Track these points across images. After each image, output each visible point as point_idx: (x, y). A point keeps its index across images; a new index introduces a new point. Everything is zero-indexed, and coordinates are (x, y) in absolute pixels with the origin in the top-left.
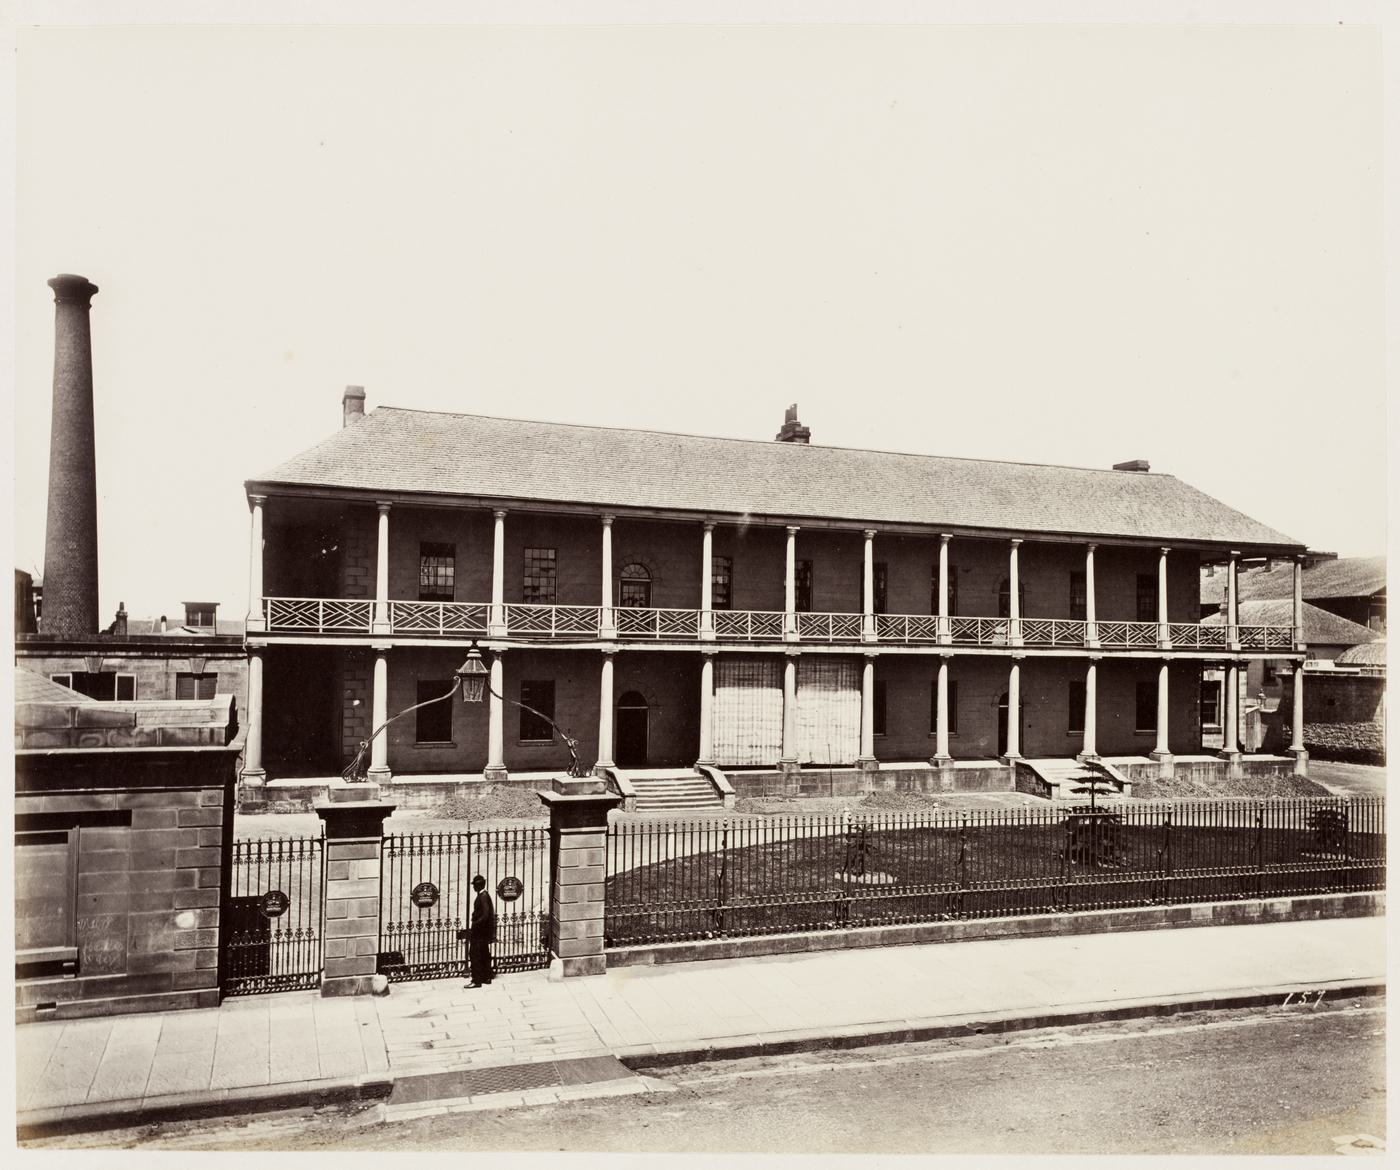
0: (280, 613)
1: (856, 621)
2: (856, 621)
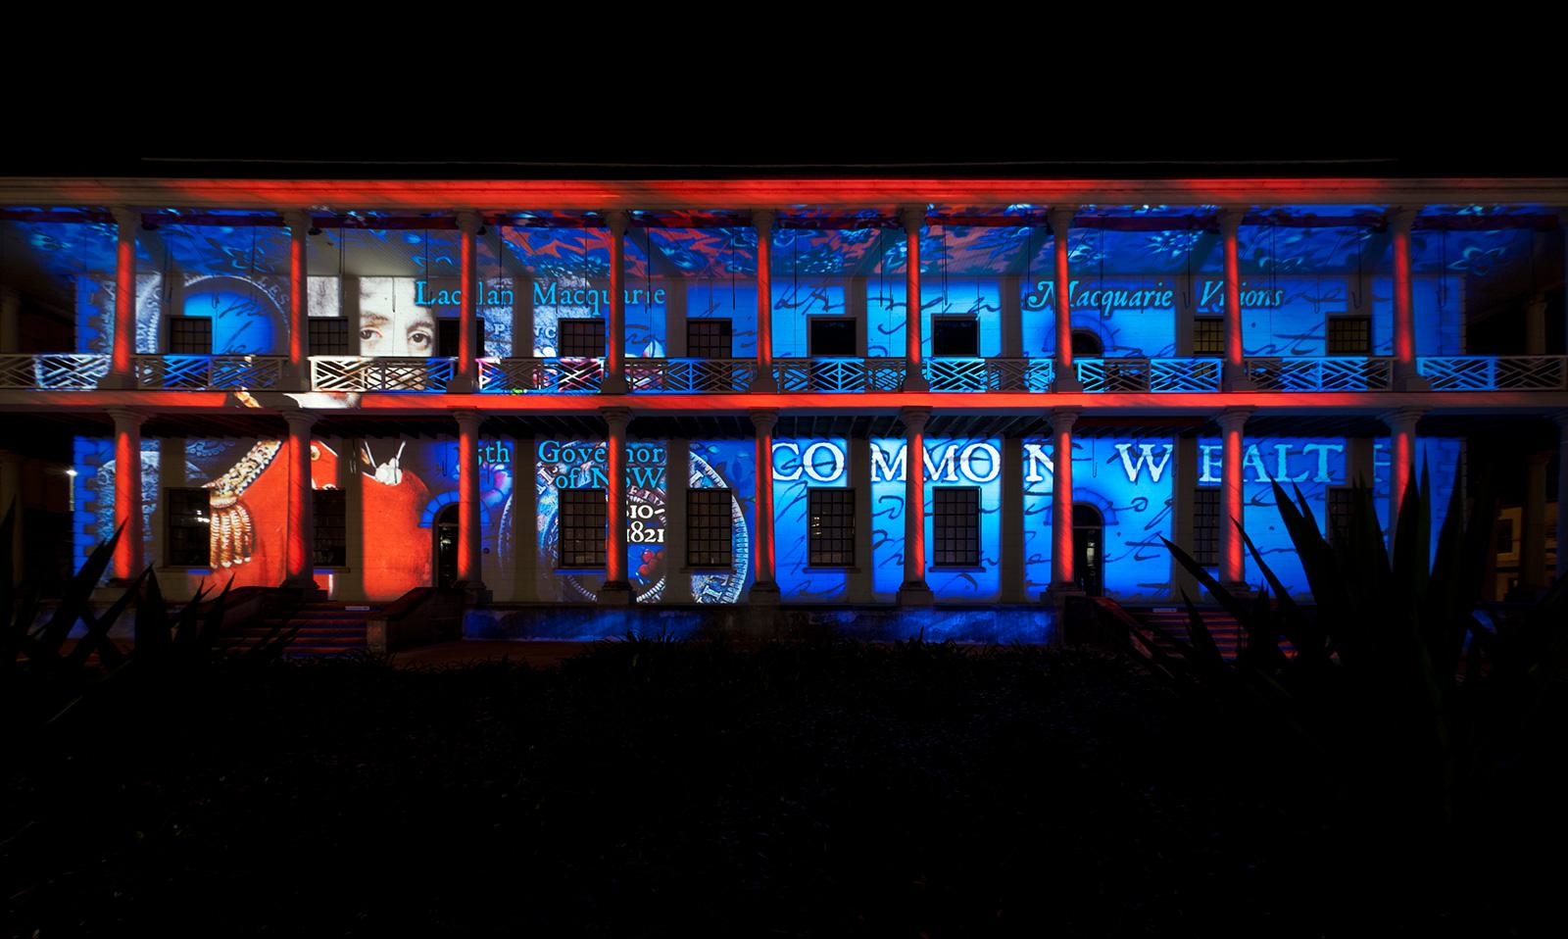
0: (1545, 377)
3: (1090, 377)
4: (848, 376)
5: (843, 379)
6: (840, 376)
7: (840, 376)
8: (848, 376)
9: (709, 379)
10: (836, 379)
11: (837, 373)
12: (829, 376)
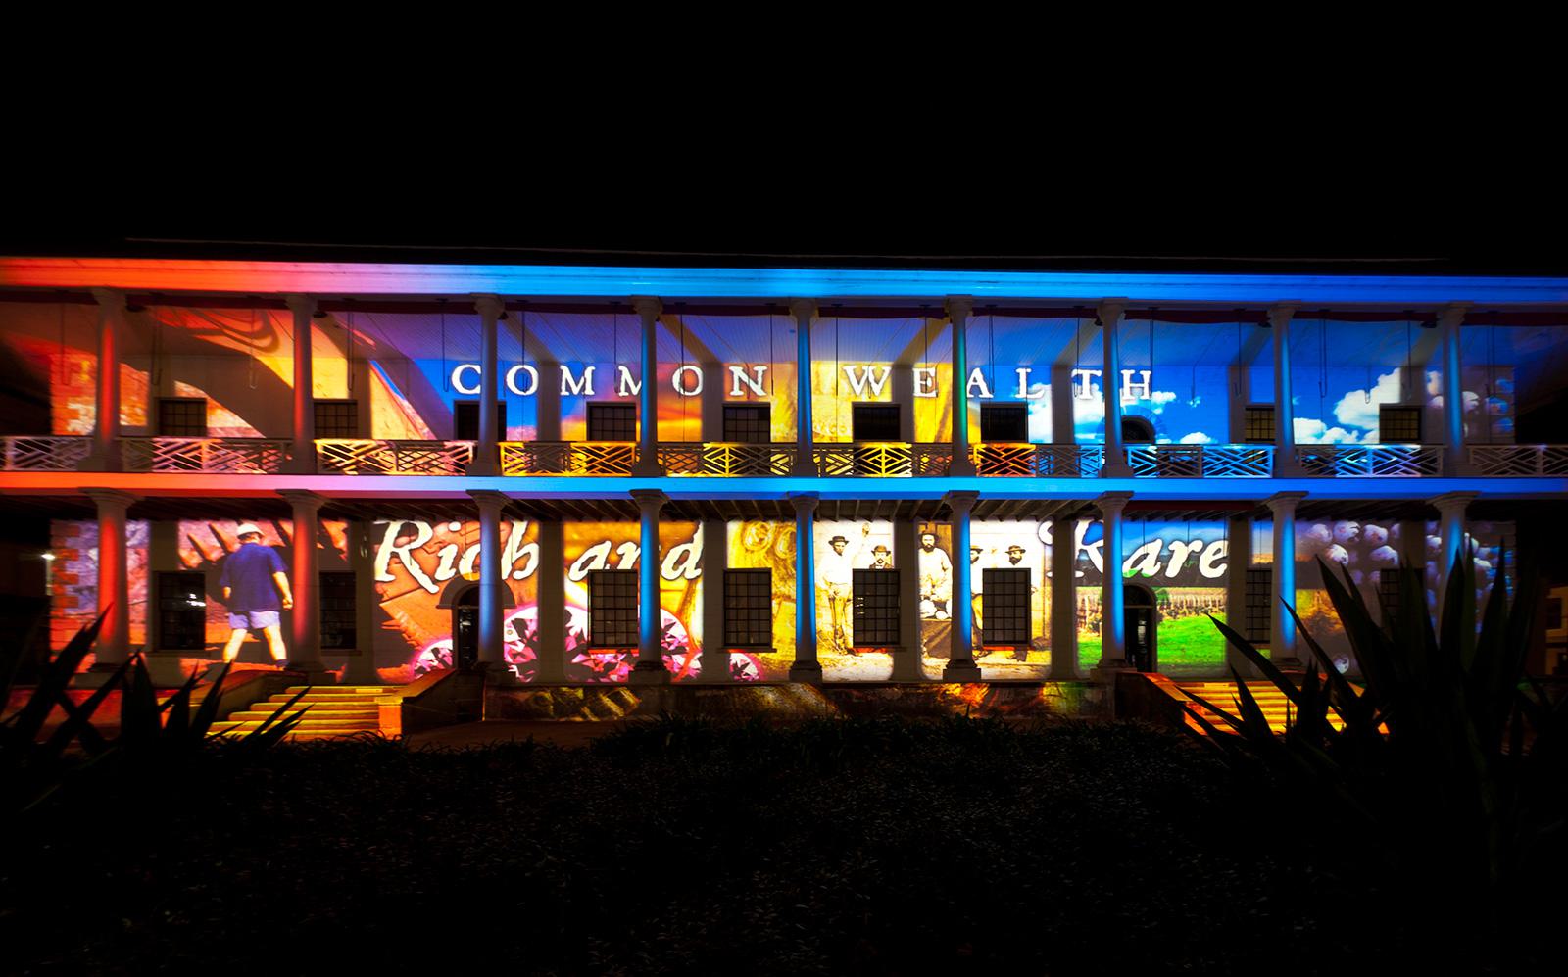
1: (23, 461)
2: (23, 461)
3: (1140, 463)
4: (892, 461)
5: (887, 464)
6: (883, 461)
7: (883, 461)
8: (892, 461)
9: (747, 463)
10: (880, 463)
11: (724, 457)
12: (873, 461)
